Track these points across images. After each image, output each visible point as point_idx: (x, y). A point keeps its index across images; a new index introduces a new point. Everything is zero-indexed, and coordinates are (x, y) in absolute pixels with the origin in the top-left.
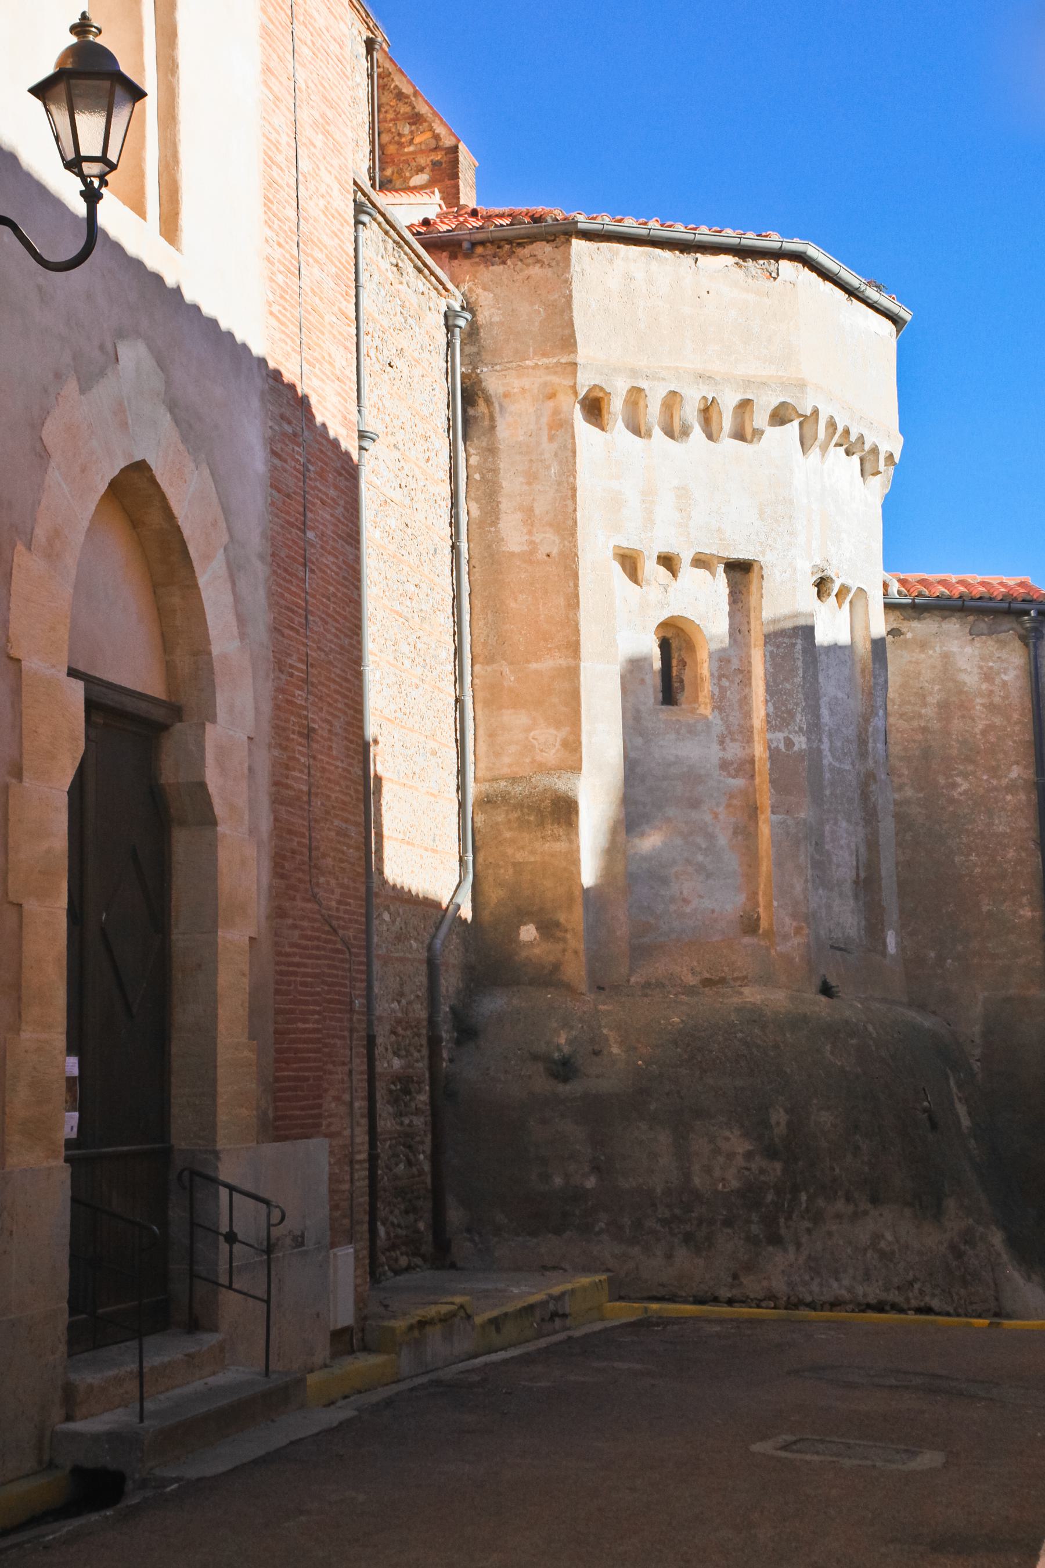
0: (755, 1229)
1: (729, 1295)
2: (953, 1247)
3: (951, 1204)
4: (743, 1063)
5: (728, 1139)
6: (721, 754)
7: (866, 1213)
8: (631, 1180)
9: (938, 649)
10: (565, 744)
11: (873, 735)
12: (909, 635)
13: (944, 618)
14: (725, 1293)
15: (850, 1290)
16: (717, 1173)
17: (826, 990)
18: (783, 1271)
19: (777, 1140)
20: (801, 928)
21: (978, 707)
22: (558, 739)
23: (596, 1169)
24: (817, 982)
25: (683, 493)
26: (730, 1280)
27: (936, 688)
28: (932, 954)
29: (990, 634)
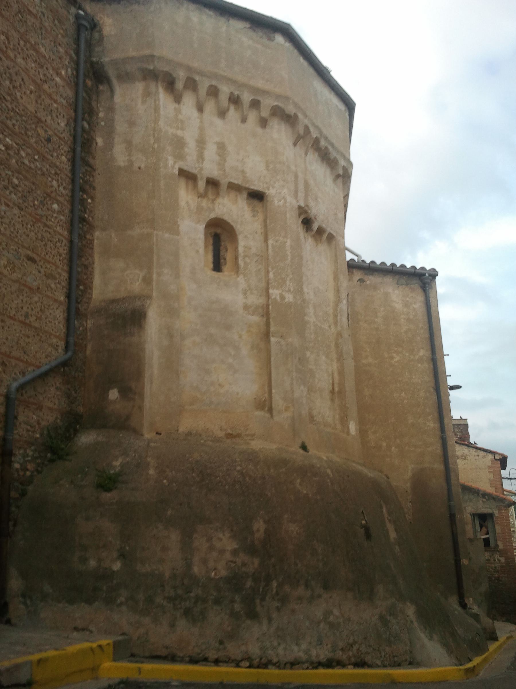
0: (237, 607)
1: (216, 656)
2: (382, 618)
3: (380, 589)
4: (237, 487)
5: (220, 540)
6: (244, 301)
7: (320, 596)
8: (147, 565)
9: (382, 290)
10: (144, 279)
11: (340, 312)
12: (368, 282)
13: (385, 275)
14: (212, 655)
15: (306, 652)
16: (211, 564)
17: (304, 447)
18: (258, 639)
19: (256, 542)
20: (289, 407)
21: (402, 320)
22: (141, 276)
23: (122, 556)
24: (299, 442)
25: (221, 147)
26: (217, 645)
27: (382, 309)
28: (385, 444)
29: (407, 284)
